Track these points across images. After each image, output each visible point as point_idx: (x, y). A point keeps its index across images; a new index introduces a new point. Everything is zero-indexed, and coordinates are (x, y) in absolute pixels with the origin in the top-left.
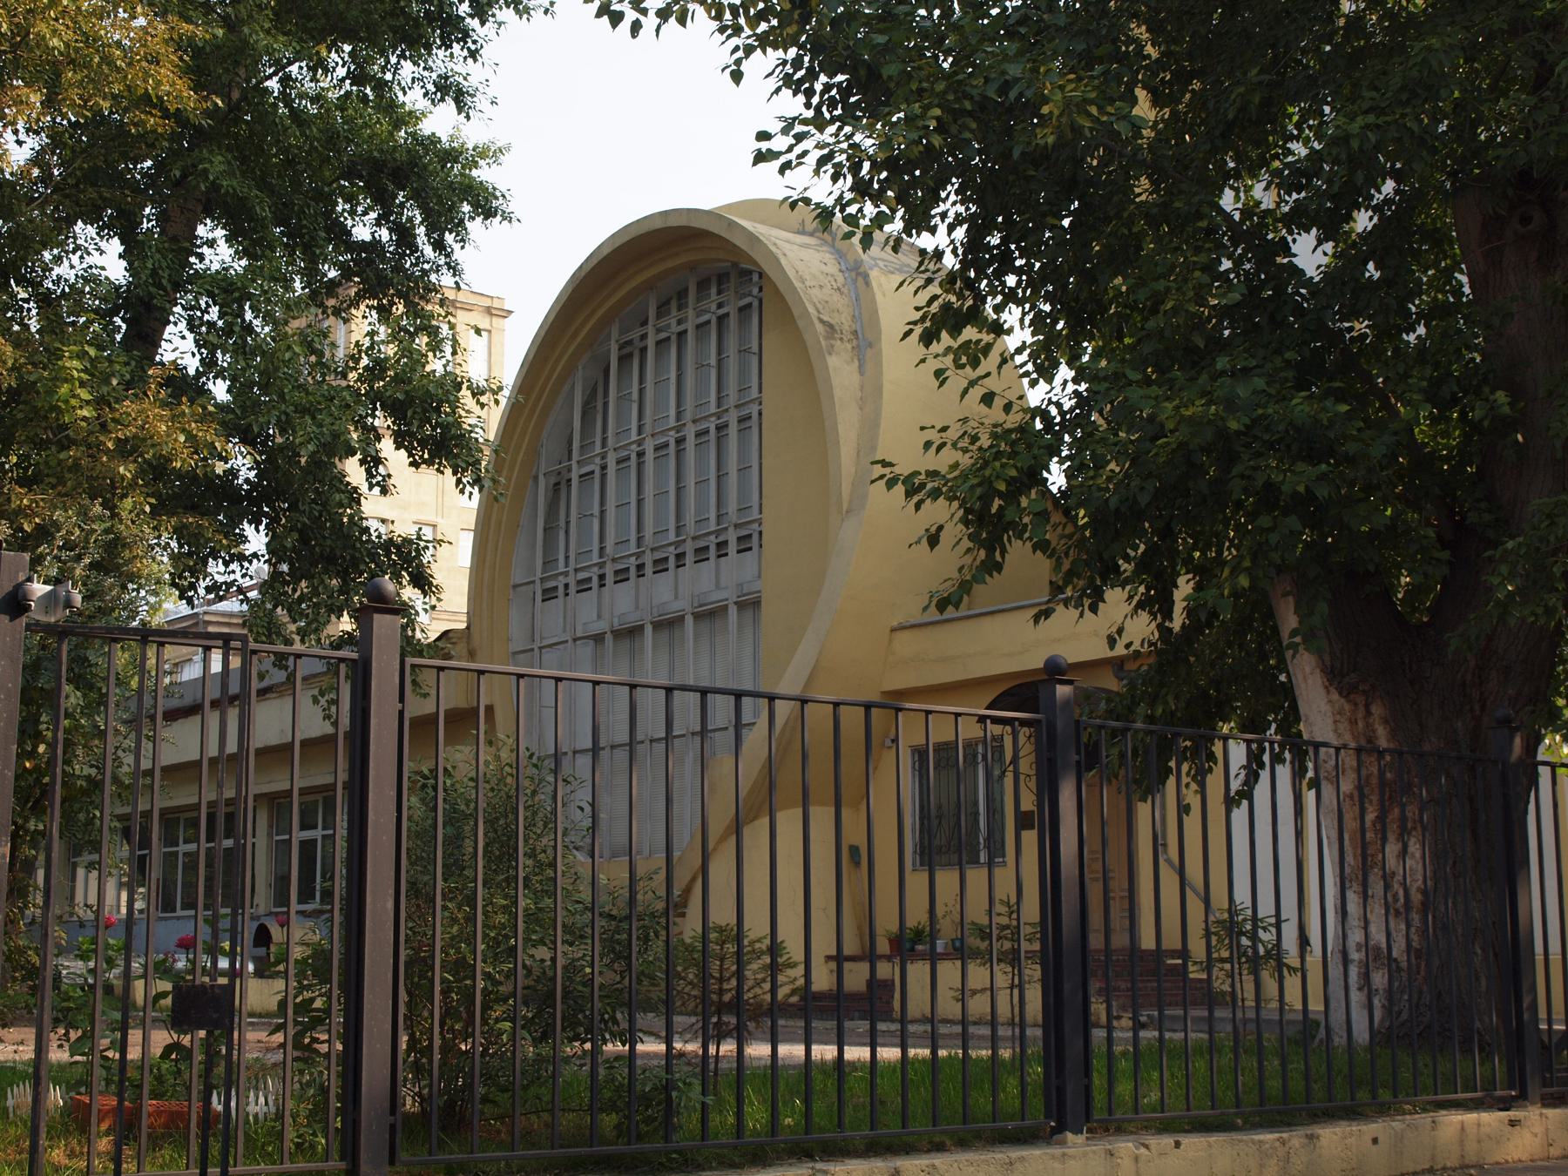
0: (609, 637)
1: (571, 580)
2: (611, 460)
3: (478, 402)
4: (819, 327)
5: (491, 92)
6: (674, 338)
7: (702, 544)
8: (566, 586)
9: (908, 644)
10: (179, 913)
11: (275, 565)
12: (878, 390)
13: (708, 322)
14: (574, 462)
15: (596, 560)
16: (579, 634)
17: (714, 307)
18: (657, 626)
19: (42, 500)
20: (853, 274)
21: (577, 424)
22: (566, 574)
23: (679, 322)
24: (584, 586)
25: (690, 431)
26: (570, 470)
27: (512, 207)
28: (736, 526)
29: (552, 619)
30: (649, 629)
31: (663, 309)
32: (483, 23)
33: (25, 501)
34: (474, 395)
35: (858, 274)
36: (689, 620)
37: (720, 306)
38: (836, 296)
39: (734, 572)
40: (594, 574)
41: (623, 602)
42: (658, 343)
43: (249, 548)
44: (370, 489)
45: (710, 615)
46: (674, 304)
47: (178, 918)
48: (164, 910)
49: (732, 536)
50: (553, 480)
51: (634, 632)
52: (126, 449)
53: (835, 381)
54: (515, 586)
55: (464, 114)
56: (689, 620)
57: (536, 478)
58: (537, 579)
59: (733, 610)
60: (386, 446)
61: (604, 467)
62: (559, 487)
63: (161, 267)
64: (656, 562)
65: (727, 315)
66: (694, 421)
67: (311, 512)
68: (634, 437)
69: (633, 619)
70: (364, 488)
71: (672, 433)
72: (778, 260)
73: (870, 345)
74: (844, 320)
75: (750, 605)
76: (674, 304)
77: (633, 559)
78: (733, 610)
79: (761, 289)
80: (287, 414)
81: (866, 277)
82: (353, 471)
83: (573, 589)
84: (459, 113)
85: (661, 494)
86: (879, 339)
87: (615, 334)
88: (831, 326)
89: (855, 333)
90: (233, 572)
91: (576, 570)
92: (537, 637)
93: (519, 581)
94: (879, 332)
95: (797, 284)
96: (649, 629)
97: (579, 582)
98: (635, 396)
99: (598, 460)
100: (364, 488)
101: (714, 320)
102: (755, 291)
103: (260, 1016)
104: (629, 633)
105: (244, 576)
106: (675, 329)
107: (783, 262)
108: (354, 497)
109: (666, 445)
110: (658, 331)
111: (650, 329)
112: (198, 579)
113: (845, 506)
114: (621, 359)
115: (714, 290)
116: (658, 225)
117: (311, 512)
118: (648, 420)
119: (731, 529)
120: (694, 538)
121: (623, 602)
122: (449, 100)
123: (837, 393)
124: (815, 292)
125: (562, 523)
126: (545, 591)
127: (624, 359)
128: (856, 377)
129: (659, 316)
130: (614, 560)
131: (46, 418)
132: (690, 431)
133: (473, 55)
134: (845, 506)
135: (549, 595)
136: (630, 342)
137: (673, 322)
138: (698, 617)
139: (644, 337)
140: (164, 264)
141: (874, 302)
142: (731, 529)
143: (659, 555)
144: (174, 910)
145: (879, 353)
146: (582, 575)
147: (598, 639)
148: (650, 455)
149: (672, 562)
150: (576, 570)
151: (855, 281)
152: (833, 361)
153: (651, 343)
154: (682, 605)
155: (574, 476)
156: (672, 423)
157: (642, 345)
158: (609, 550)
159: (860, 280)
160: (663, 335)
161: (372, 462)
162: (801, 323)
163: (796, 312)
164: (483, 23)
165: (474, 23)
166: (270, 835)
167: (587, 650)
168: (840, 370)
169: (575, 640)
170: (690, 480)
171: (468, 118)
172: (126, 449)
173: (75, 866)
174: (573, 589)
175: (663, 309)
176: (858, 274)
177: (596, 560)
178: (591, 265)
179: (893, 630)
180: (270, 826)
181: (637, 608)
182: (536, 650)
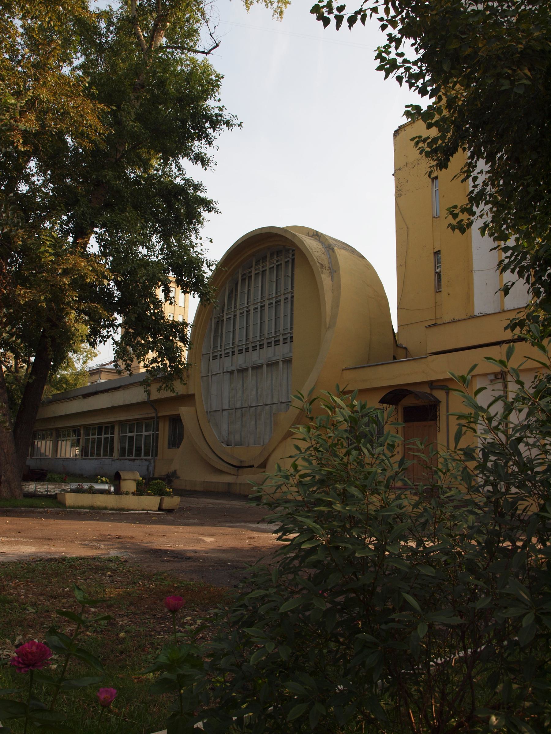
0: (236, 372)
1: (223, 353)
2: (238, 313)
3: (210, 269)
4: (318, 264)
5: (215, 160)
6: (261, 273)
7: (269, 341)
8: (221, 355)
9: (348, 375)
10: (90, 457)
11: (127, 329)
12: (339, 286)
13: (273, 267)
14: (225, 314)
15: (231, 346)
16: (225, 371)
17: (275, 262)
18: (253, 368)
19: (30, 292)
20: (328, 249)
21: (226, 301)
22: (221, 351)
23: (263, 267)
24: (227, 355)
25: (267, 303)
26: (223, 316)
27: (217, 206)
28: (283, 335)
29: (215, 366)
30: (250, 369)
31: (257, 263)
32: (214, 131)
33: (22, 292)
34: (208, 266)
35: (330, 249)
36: (265, 366)
37: (277, 261)
38: (323, 255)
39: (281, 351)
40: (230, 351)
41: (240, 360)
42: (255, 274)
43: (117, 322)
44: (166, 302)
45: (272, 365)
46: (261, 261)
47: (89, 459)
48: (85, 456)
49: (281, 338)
50: (217, 320)
51: (246, 370)
52: (66, 272)
53: (324, 283)
54: (203, 355)
55: (204, 168)
56: (265, 366)
57: (211, 319)
58: (211, 352)
59: (281, 363)
60: (173, 285)
61: (235, 316)
62: (219, 322)
63: (86, 213)
64: (253, 347)
65: (281, 264)
66: (268, 299)
67: (142, 307)
68: (246, 305)
69: (244, 366)
70: (163, 301)
71: (259, 304)
72: (303, 242)
73: (335, 272)
74: (326, 263)
75: (288, 361)
76: (261, 261)
77: (244, 346)
78: (281, 363)
79: (293, 255)
80: (134, 267)
81: (333, 250)
82: (160, 294)
83: (223, 356)
84: (203, 167)
85: (255, 324)
86: (339, 269)
87: (240, 272)
88: (322, 265)
89: (329, 267)
90: (111, 331)
91: (225, 349)
92: (210, 372)
93: (205, 353)
94: (339, 267)
95: (310, 250)
96: (250, 369)
97: (226, 354)
98: (246, 292)
99: (232, 313)
100: (163, 301)
101: (275, 266)
102: (291, 256)
103: (116, 510)
104: (243, 371)
105: (115, 333)
106: (261, 269)
107: (305, 242)
108: (158, 304)
109: (257, 308)
110: (256, 270)
111: (253, 269)
112: (97, 338)
113: (327, 326)
114: (242, 280)
115: (275, 256)
116: (259, 232)
117: (142, 307)
118: (251, 299)
119: (281, 336)
120: (267, 339)
121: (240, 360)
122: (199, 162)
123: (325, 287)
124: (316, 253)
125: (220, 334)
126: (213, 357)
127: (243, 280)
128: (331, 282)
129: (256, 265)
130: (238, 346)
131: (35, 262)
132: (267, 303)
133: (210, 143)
134: (327, 326)
135: (215, 358)
136: (245, 274)
137: (261, 267)
138: (268, 365)
139: (250, 272)
140: (88, 212)
141: (336, 258)
142: (281, 336)
143: (254, 345)
144: (88, 456)
145: (339, 274)
146: (226, 351)
147: (232, 372)
148: (252, 311)
149: (258, 348)
150: (225, 349)
151: (328, 251)
152: (323, 276)
153: (253, 274)
154: (262, 361)
155: (225, 319)
156: (259, 300)
157: (249, 275)
158: (237, 342)
159: (331, 251)
160: (257, 272)
161: (167, 291)
162: (311, 263)
163: (310, 259)
164: (214, 131)
165: (210, 131)
166: (119, 434)
167: (227, 376)
168: (326, 279)
169: (224, 373)
170: (266, 319)
171: (206, 169)
172: (66, 272)
173: (58, 441)
174: (223, 356)
175: (257, 263)
176: (330, 249)
177: (231, 346)
178: (234, 247)
179: (343, 370)
180: (119, 431)
181: (245, 362)
182: (210, 376)
